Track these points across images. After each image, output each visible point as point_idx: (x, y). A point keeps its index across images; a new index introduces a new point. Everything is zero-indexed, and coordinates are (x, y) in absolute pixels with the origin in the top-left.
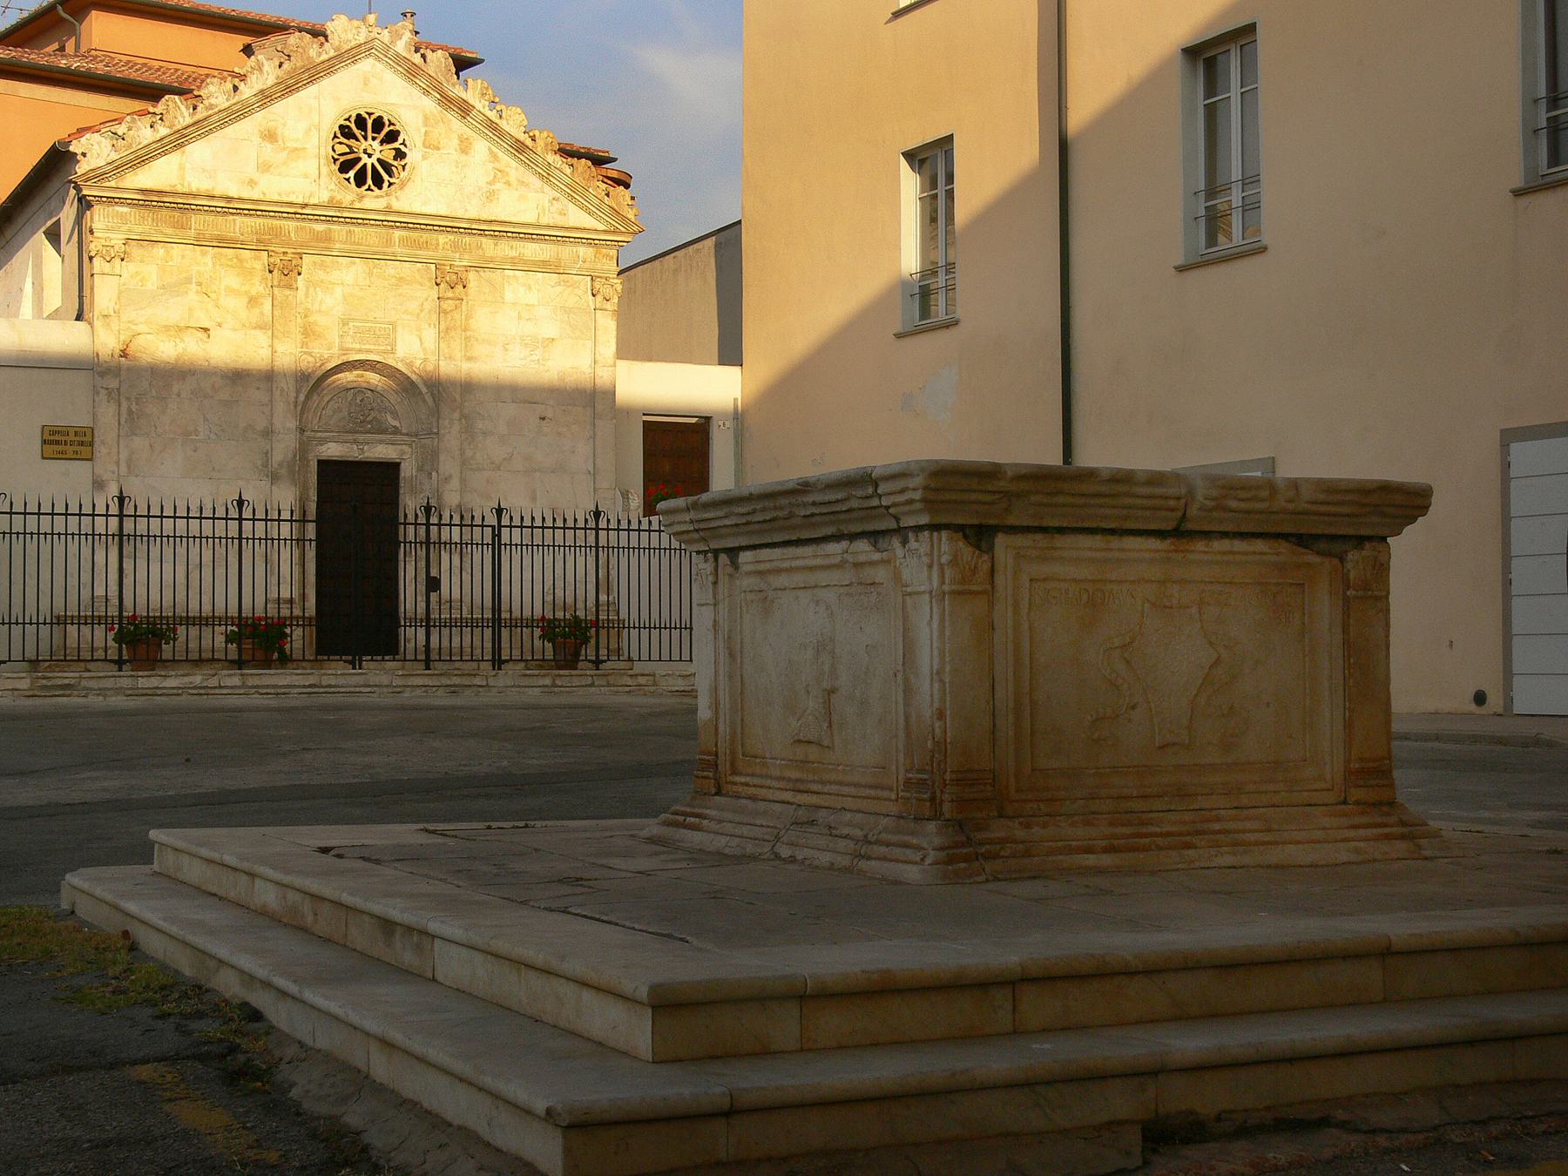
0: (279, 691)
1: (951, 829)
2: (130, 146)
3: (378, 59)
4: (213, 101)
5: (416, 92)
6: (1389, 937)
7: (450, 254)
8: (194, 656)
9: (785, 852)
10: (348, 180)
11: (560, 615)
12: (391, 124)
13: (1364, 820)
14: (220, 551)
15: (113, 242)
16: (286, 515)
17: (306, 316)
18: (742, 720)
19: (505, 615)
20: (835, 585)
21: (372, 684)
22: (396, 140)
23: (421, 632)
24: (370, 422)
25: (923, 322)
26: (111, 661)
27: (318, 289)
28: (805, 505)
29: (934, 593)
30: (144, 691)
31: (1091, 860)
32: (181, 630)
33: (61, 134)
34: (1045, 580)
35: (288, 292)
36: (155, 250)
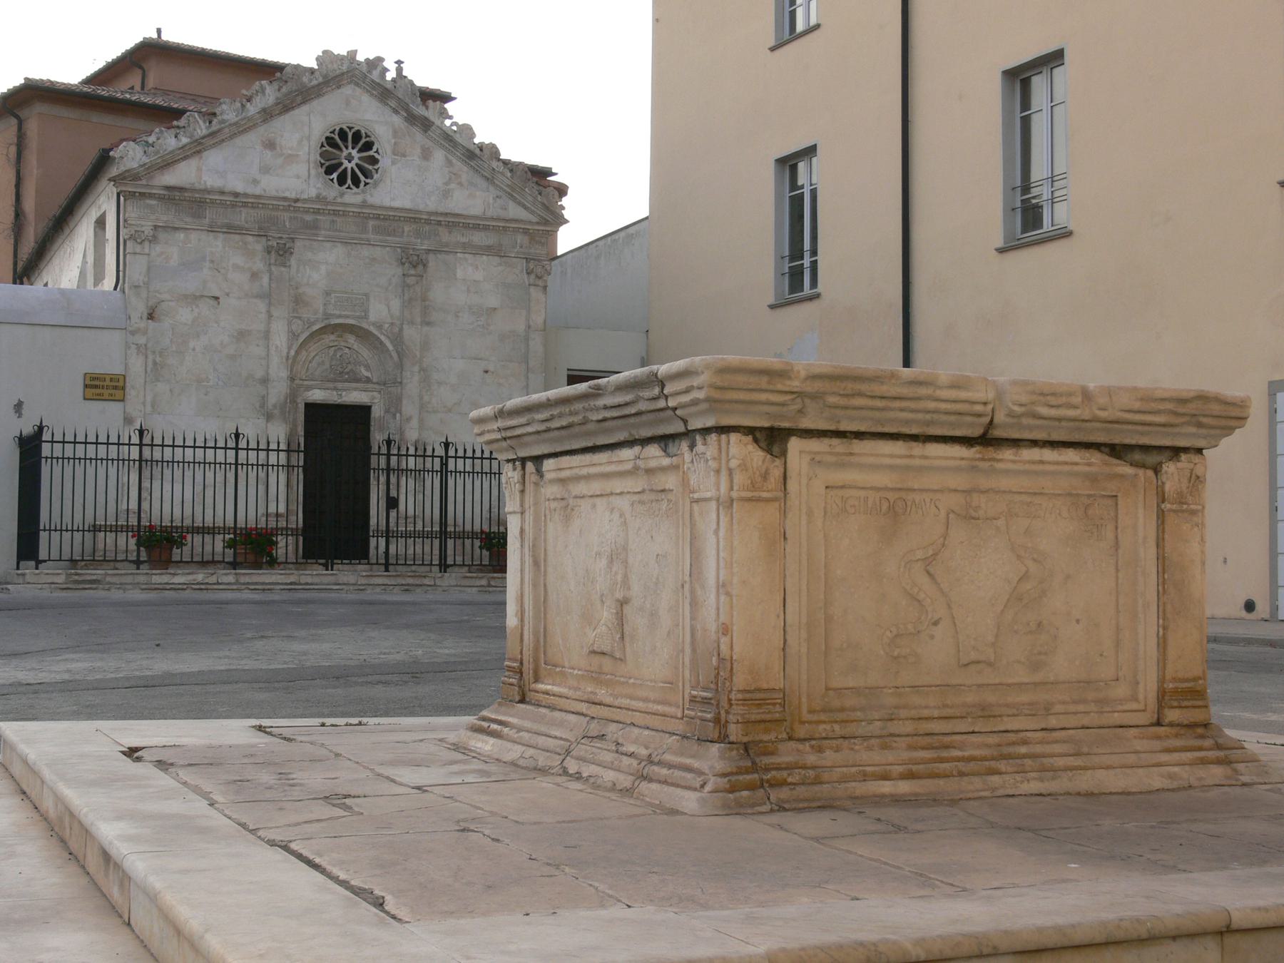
1: (735, 752)
2: (158, 152)
3: (357, 84)
4: (225, 117)
5: (388, 111)
6: (1227, 910)
7: (413, 240)
8: (110, 556)
9: (572, 766)
10: (332, 180)
12: (367, 136)
13: (1178, 743)
15: (143, 229)
17: (297, 288)
19: (450, 529)
20: (629, 493)
21: (341, 582)
22: (370, 149)
23: (382, 541)
26: (131, 561)
28: (597, 409)
29: (721, 500)
30: (156, 586)
31: (886, 787)
32: (189, 537)
33: (107, 146)
34: (842, 487)
35: (283, 269)
36: (177, 235)
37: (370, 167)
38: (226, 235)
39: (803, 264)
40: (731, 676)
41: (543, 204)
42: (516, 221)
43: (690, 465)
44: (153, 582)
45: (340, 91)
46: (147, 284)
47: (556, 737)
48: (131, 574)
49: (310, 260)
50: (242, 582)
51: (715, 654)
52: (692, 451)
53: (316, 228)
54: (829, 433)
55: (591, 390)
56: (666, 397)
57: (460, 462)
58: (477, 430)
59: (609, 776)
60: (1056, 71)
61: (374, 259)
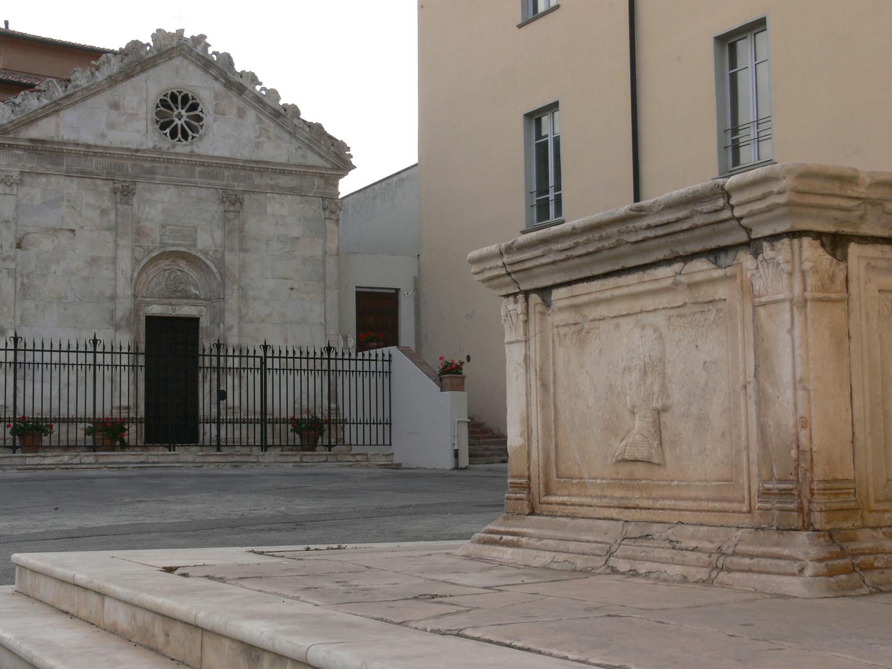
0: (121, 466)
2: (23, 111)
3: (185, 57)
4: (78, 83)
7: (232, 182)
10: (166, 134)
11: (305, 416)
12: (193, 98)
14: (81, 374)
16: (125, 350)
17: (138, 222)
18: (556, 446)
20: (664, 308)
22: (196, 109)
24: (180, 291)
25: (540, 223)
27: (146, 205)
28: (636, 231)
29: (795, 301)
32: (55, 426)
35: (127, 207)
37: (196, 124)
38: (80, 179)
39: (549, 197)
40: (812, 467)
41: (335, 153)
42: (314, 167)
43: (755, 272)
44: (27, 463)
45: (170, 62)
46: (15, 219)
47: (589, 542)
48: (8, 457)
49: (149, 199)
50: (101, 462)
51: (794, 446)
52: (756, 258)
53: (153, 173)
54: (880, 240)
55: (633, 212)
56: (732, 207)
57: (276, 361)
58: (474, 269)
59: (675, 571)
60: (759, 36)
61: (200, 198)
